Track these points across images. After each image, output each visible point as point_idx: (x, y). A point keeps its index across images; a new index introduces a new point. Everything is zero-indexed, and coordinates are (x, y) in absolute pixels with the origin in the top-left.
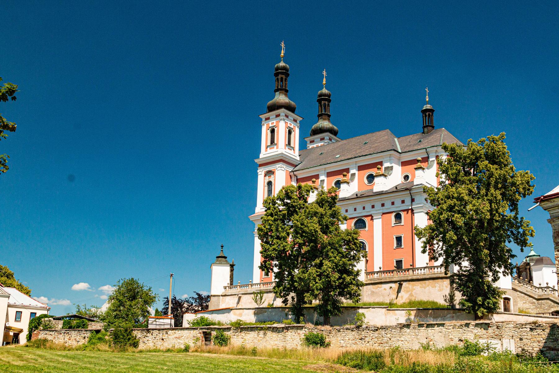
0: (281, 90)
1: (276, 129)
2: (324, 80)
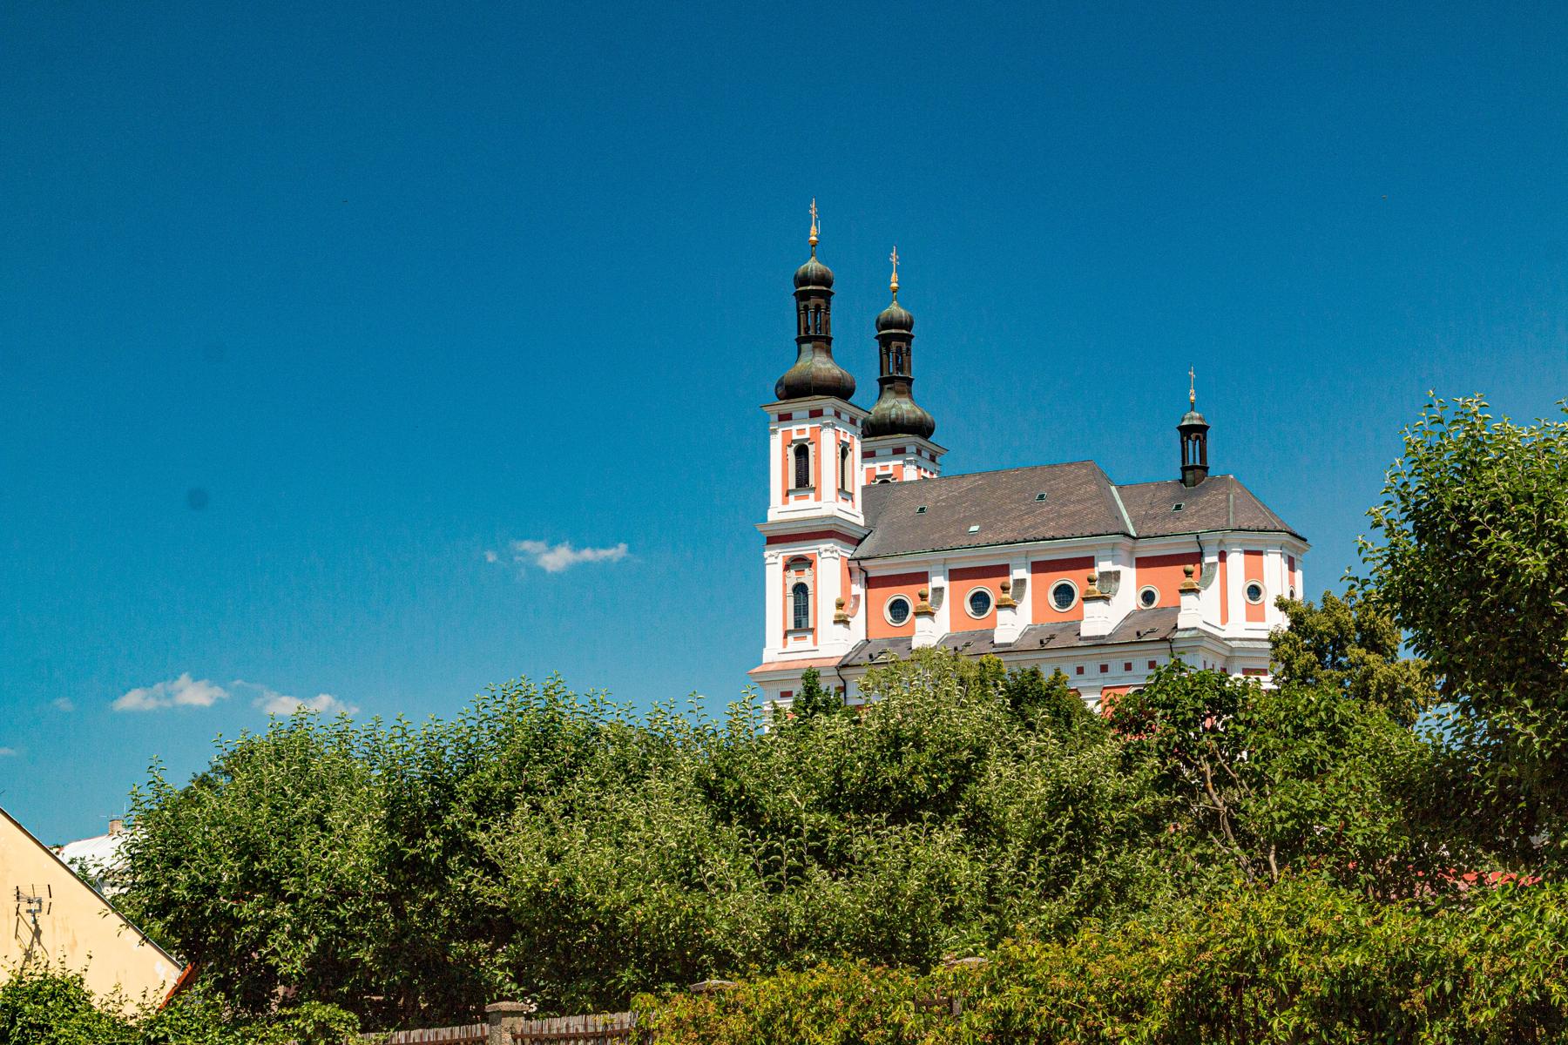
0: (816, 338)
1: (811, 448)
2: (894, 276)
